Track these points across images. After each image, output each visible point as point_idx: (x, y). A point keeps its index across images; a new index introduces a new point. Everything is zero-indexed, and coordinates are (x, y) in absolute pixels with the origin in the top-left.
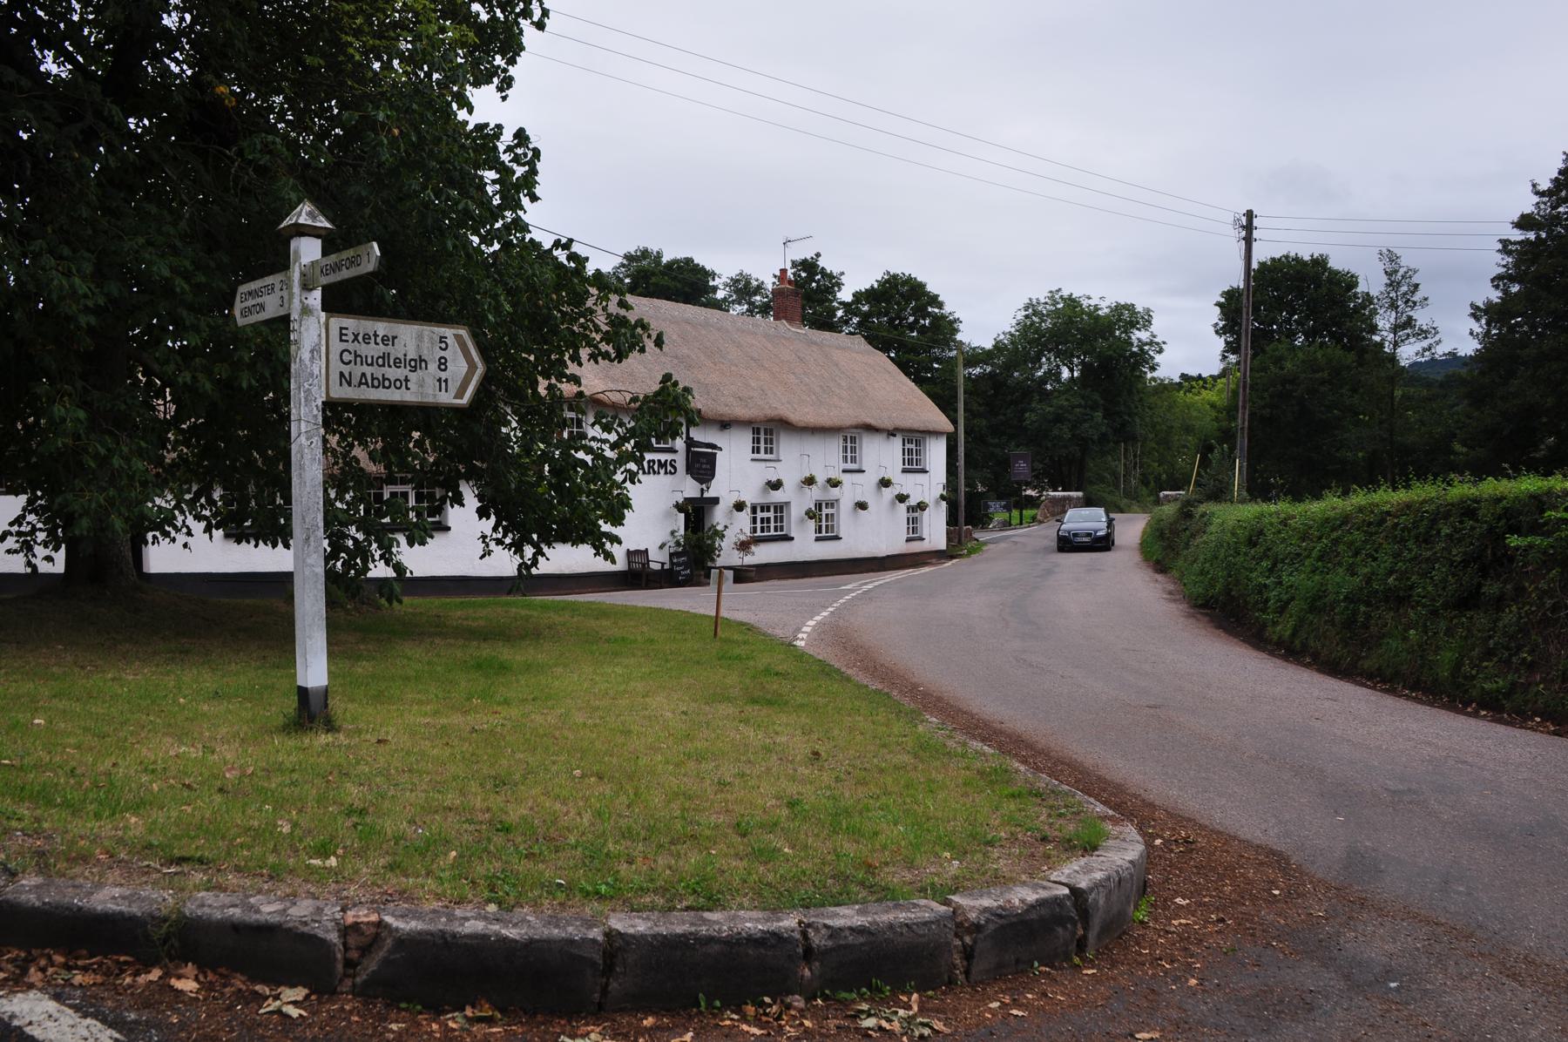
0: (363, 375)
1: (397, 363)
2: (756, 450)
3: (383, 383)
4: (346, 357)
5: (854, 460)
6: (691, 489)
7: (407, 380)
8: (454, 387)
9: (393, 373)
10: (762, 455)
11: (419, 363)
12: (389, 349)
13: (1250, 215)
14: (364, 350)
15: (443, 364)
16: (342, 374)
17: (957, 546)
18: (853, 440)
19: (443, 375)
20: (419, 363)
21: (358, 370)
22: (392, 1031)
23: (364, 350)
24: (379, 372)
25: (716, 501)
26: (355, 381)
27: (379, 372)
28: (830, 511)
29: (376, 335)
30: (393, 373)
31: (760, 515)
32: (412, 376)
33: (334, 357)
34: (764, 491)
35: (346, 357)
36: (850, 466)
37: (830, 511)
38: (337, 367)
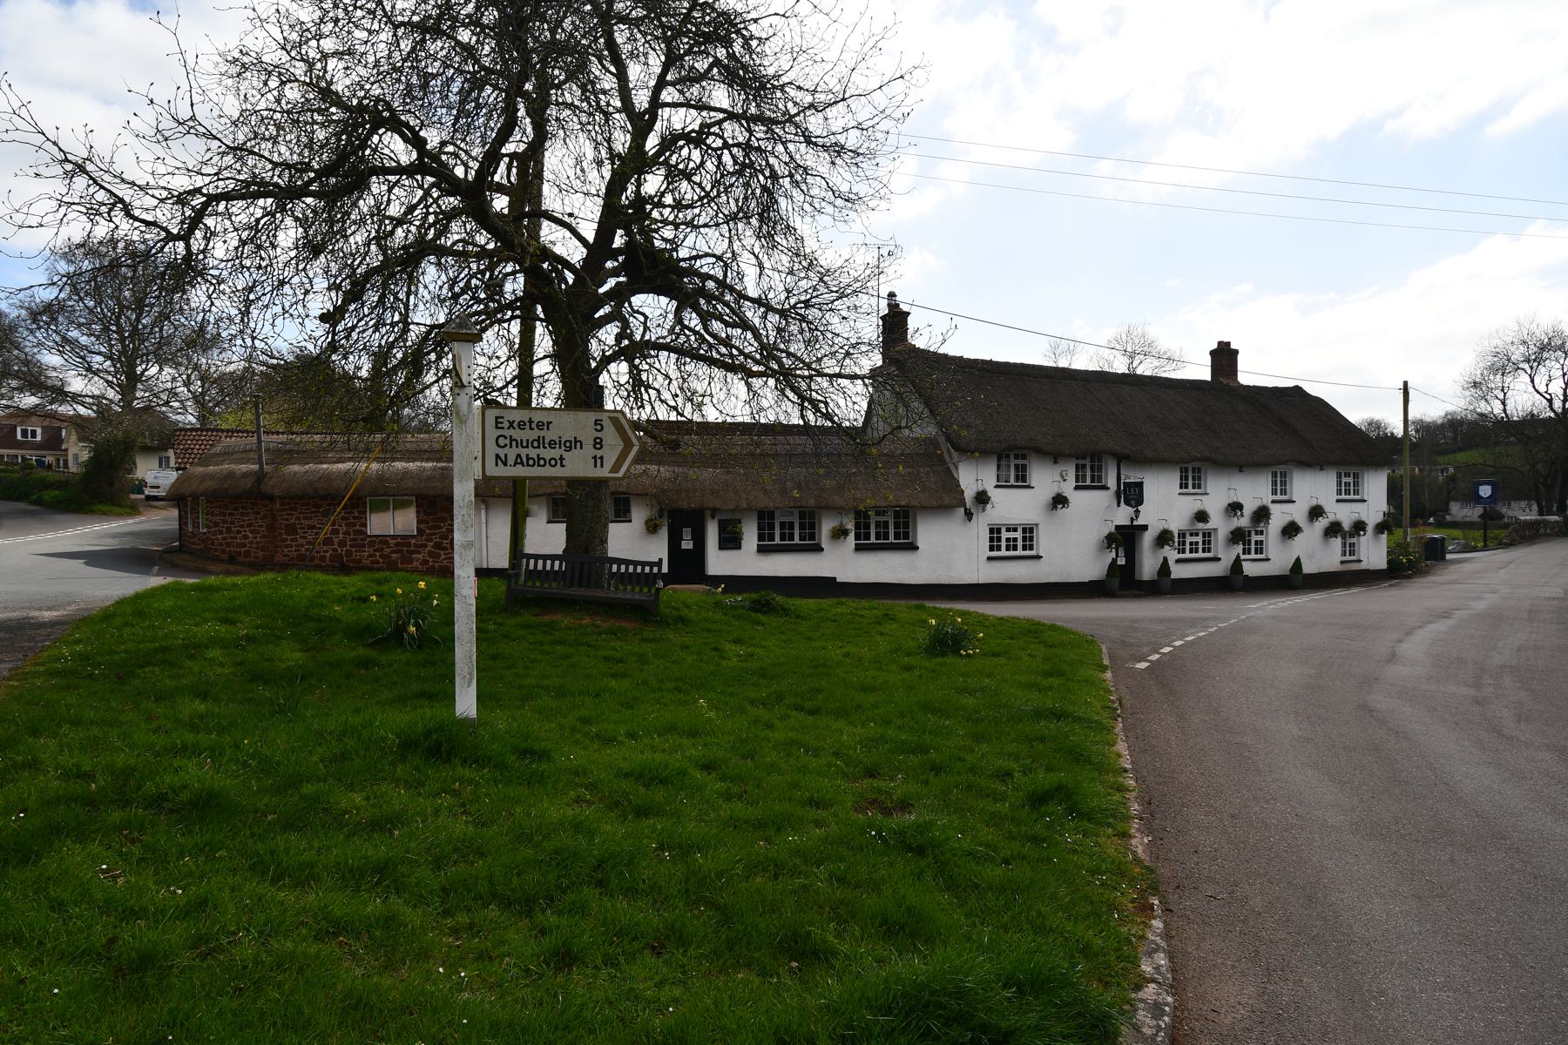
0: (519, 456)
1: (552, 444)
2: (1183, 485)
3: (539, 462)
4: (502, 441)
5: (1284, 492)
6: (1123, 515)
7: (562, 459)
8: (609, 464)
9: (547, 453)
10: (1190, 490)
11: (573, 444)
12: (542, 434)
13: (1406, 383)
14: (517, 434)
15: (598, 443)
16: (497, 456)
17: (1398, 570)
18: (1284, 475)
19: (599, 453)
20: (573, 444)
21: (512, 454)
22: (615, 273)
23: (517, 434)
24: (533, 453)
25: (1145, 528)
26: (511, 461)
27: (533, 453)
28: (1259, 538)
29: (530, 421)
30: (547, 453)
31: (1189, 539)
32: (565, 455)
33: (491, 443)
34: (1192, 523)
35: (502, 441)
36: (1279, 497)
37: (1259, 538)
38: (492, 449)
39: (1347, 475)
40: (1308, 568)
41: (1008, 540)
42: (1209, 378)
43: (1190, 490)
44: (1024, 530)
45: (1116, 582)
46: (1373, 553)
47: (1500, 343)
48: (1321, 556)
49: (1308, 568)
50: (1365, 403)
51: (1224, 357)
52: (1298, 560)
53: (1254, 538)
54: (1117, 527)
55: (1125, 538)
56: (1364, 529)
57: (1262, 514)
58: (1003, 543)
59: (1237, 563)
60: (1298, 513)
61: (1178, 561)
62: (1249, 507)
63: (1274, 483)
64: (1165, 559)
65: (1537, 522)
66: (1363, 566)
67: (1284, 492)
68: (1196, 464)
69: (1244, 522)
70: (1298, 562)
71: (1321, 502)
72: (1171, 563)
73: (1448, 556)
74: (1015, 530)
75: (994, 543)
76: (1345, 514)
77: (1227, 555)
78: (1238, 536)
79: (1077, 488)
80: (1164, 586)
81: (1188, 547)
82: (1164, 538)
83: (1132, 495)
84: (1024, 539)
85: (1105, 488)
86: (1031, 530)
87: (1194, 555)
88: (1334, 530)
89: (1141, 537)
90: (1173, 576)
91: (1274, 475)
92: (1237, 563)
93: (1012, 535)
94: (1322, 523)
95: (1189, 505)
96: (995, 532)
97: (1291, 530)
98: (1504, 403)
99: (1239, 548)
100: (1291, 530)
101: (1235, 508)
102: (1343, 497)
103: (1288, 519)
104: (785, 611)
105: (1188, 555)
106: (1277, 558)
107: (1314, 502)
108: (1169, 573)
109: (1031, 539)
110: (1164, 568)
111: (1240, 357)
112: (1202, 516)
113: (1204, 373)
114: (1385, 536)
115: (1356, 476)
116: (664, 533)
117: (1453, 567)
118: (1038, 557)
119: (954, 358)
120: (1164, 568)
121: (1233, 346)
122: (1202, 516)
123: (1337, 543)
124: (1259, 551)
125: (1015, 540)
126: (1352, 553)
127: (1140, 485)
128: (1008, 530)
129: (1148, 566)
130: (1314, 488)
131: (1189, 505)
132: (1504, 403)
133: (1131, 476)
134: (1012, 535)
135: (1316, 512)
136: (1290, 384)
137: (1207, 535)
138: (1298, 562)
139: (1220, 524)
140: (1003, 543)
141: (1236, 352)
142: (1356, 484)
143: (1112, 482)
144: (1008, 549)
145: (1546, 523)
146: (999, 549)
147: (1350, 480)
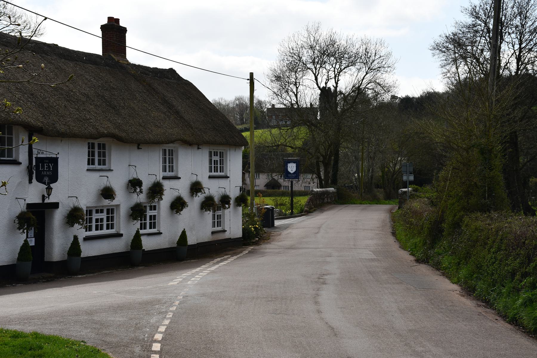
2: (91, 162)
6: (34, 193)
13: (252, 74)
18: (171, 153)
25: (56, 205)
28: (153, 213)
31: (95, 216)
34: (99, 200)
36: (168, 174)
37: (153, 213)
39: (216, 154)
40: (191, 240)
42: (99, 51)
43: (96, 166)
44: (108, 210)
45: (28, 265)
46: (233, 224)
47: (293, 45)
48: (197, 227)
49: (191, 240)
50: (221, 90)
51: (114, 33)
52: (184, 233)
53: (149, 213)
54: (29, 206)
55: (35, 218)
56: (228, 203)
57: (156, 190)
59: (137, 239)
61: (86, 239)
62: (146, 184)
63: (91, 154)
64: (76, 238)
65: (323, 193)
66: (227, 235)
67: (172, 169)
68: (102, 140)
69: (142, 198)
70: (184, 235)
71: (200, 179)
72: (80, 240)
73: (277, 223)
74: (102, 211)
76: (214, 189)
77: (127, 229)
78: (137, 212)
79: (210, 177)
80: (76, 268)
81: (94, 224)
82: (74, 216)
83: (45, 171)
85: (16, 163)
86: (112, 210)
87: (99, 232)
88: (208, 204)
89: (51, 216)
90: (83, 255)
91: (91, 146)
92: (137, 239)
94: (200, 198)
95: (94, 182)
97: (178, 205)
98: (296, 96)
99: (138, 224)
100: (178, 205)
101: (134, 184)
102: (213, 174)
103: (176, 194)
105: (94, 233)
106: (167, 231)
107: (194, 179)
108: (79, 252)
109: (112, 218)
110: (75, 248)
111: (128, 35)
112: (107, 193)
113: (95, 47)
114: (240, 209)
115: (221, 155)
117: (285, 232)
118: (160, 233)
119: (49, 46)
120: (75, 248)
121: (122, 24)
122: (107, 193)
123: (209, 215)
124: (153, 225)
125: (102, 220)
126: (219, 224)
127: (55, 161)
128: (97, 212)
129: (58, 247)
130: (193, 165)
131: (94, 182)
132: (296, 96)
133: (45, 149)
135: (196, 188)
136: (164, 65)
137: (110, 211)
138: (184, 235)
139: (123, 201)
141: (124, 30)
142: (222, 162)
143: (23, 156)
144: (97, 229)
145: (327, 193)
147: (217, 158)
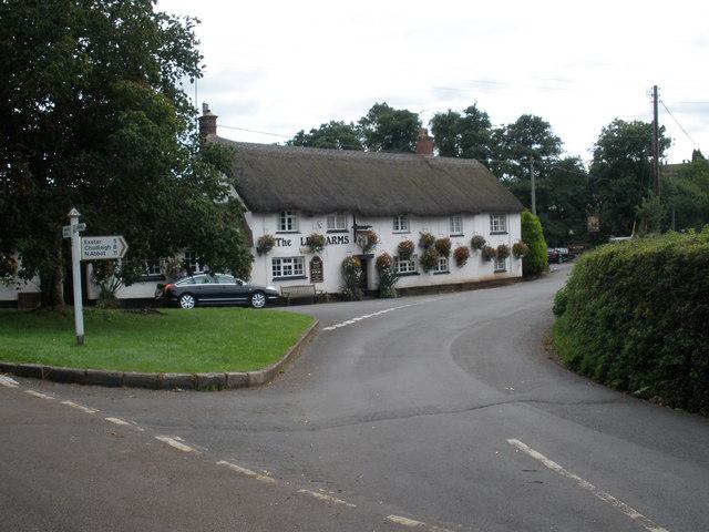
5: (458, 230)
13: (655, 88)
41: (285, 268)
58: (282, 271)
60: (465, 242)
74: (290, 261)
75: (276, 269)
76: (494, 243)
84: (296, 267)
93: (287, 264)
96: (276, 261)
104: (159, 313)
116: (660, 126)
119: (109, 235)
125: (290, 267)
128: (285, 261)
134: (287, 264)
136: (402, 108)
140: (282, 271)
146: (279, 274)
